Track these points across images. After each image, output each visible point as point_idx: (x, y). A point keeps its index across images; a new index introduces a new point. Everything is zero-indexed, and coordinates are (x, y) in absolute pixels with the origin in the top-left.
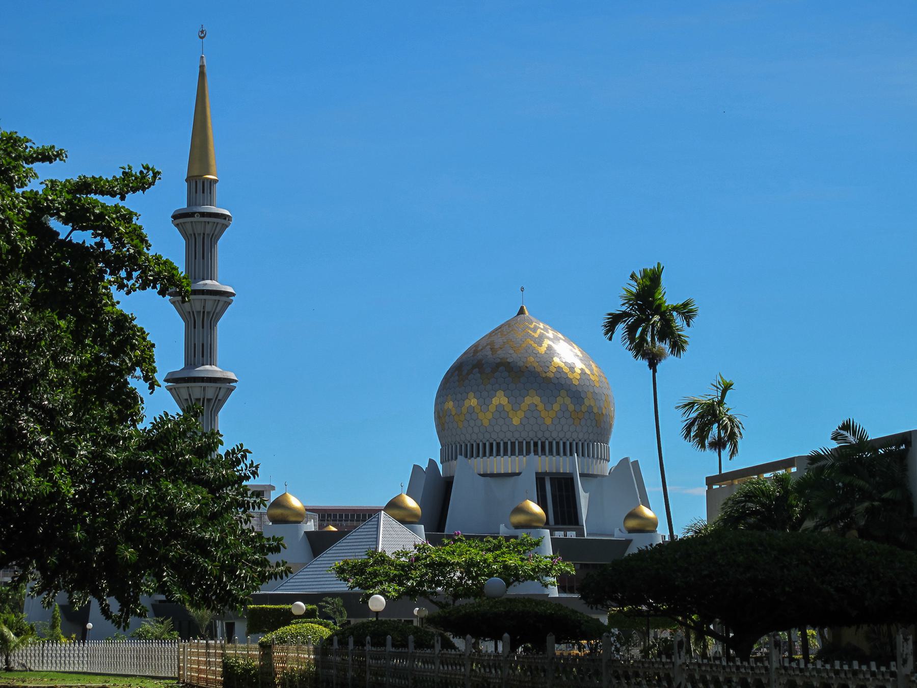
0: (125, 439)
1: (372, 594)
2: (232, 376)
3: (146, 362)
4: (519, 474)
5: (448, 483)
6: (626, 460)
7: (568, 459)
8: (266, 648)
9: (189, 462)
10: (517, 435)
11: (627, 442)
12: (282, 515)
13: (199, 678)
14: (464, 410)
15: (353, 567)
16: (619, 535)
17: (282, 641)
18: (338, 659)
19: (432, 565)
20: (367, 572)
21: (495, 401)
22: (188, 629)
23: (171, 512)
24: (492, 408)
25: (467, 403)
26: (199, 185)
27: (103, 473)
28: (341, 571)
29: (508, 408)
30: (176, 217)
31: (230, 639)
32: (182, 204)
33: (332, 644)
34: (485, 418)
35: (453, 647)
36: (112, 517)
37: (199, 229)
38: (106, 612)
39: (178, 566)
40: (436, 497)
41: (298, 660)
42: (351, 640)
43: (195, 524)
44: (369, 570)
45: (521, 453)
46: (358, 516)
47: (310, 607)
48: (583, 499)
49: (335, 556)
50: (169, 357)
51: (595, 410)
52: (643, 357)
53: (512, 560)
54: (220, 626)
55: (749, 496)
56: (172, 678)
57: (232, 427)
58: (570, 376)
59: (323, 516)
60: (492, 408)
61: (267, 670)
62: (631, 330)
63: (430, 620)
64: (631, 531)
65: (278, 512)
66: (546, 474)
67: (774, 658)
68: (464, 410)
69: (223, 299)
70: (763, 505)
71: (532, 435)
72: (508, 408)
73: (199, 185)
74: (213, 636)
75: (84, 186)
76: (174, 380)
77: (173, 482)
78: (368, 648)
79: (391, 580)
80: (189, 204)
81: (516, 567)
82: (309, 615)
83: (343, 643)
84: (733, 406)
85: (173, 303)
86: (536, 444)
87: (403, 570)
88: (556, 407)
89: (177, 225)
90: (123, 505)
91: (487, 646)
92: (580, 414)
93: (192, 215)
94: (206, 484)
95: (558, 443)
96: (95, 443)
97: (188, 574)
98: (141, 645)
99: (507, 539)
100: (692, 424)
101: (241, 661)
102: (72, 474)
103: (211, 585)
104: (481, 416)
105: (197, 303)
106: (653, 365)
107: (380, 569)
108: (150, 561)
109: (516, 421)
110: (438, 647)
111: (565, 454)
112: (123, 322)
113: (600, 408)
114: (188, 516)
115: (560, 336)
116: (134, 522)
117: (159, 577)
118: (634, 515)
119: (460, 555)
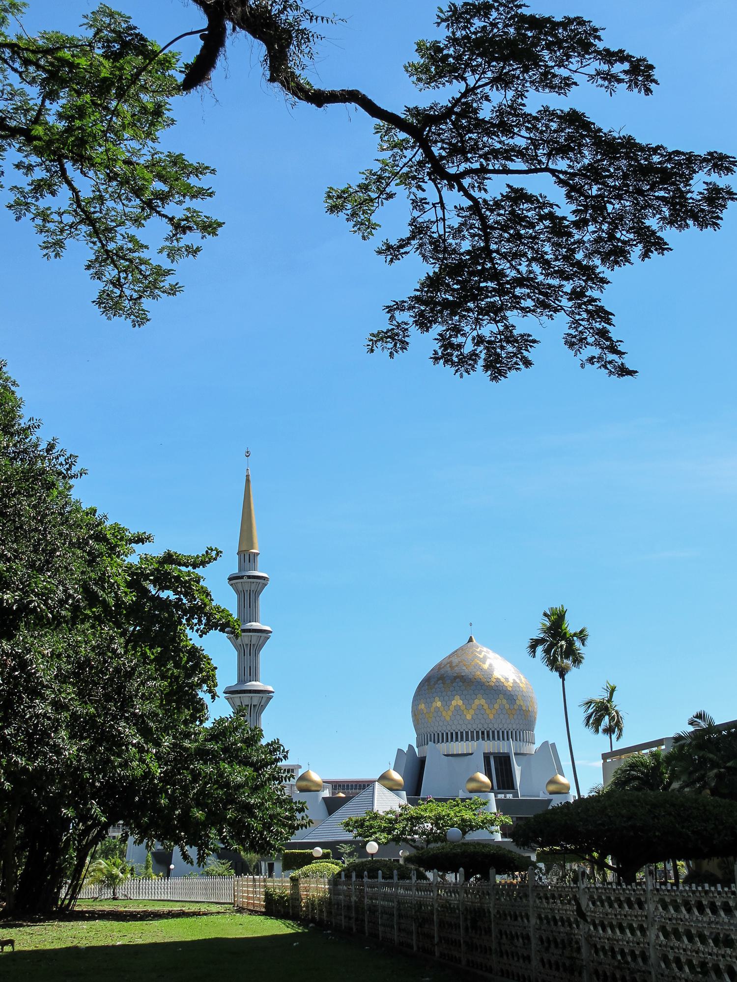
0: (195, 734)
1: (368, 841)
2: (270, 688)
3: (209, 679)
4: (471, 754)
5: (422, 762)
6: (547, 742)
7: (506, 743)
8: (294, 880)
9: (241, 749)
10: (470, 727)
11: (546, 730)
12: (307, 786)
13: (248, 903)
14: (432, 710)
15: (356, 822)
16: (543, 796)
17: (306, 875)
18: (345, 888)
19: (411, 819)
20: (364, 827)
21: (454, 703)
22: (241, 868)
23: (227, 785)
24: (452, 708)
25: (434, 705)
26: (247, 557)
27: (181, 759)
28: (347, 824)
29: (463, 707)
30: (230, 579)
31: (270, 876)
32: (235, 570)
33: (340, 878)
34: (447, 715)
35: (426, 878)
36: (186, 789)
37: (246, 588)
38: (185, 857)
39: (232, 823)
40: (415, 774)
41: (317, 889)
42: (354, 875)
43: (244, 793)
44: (367, 823)
45: (473, 739)
46: (360, 786)
47: (326, 851)
48: (517, 771)
49: (345, 813)
50: (227, 675)
51: (524, 708)
52: (556, 670)
53: (468, 815)
54: (264, 866)
55: (633, 766)
56: (230, 904)
57: (271, 726)
58: (506, 684)
59: (335, 786)
60: (452, 708)
61: (295, 897)
62: (547, 651)
63: (407, 860)
64: (551, 793)
65: (303, 784)
66: (491, 753)
67: (649, 883)
68: (432, 710)
69: (264, 635)
70: (643, 773)
71: (480, 726)
72: (463, 707)
73: (247, 557)
74: (259, 873)
75: (169, 558)
76: (230, 692)
77: (229, 763)
78: (366, 880)
79: (383, 831)
80: (240, 570)
81: (470, 821)
82: (325, 856)
83: (348, 876)
84: (619, 703)
85: (229, 638)
86: (483, 733)
87: (391, 823)
88: (496, 706)
89: (231, 585)
90: (195, 779)
91: (450, 877)
92: (511, 713)
93: (242, 577)
94: (252, 765)
95: (498, 732)
96: (174, 737)
97: (240, 830)
98: (209, 880)
99: (463, 800)
100: (589, 717)
101: (277, 891)
102: (158, 757)
103: (255, 838)
104: (444, 713)
105: (245, 638)
106: (562, 676)
107: (375, 823)
108: (215, 819)
109: (469, 717)
110: (414, 878)
111: (503, 739)
112: (195, 654)
113: (527, 706)
114: (239, 786)
115: (497, 656)
116: (201, 792)
117: (220, 832)
118: (553, 782)
119: (431, 811)
